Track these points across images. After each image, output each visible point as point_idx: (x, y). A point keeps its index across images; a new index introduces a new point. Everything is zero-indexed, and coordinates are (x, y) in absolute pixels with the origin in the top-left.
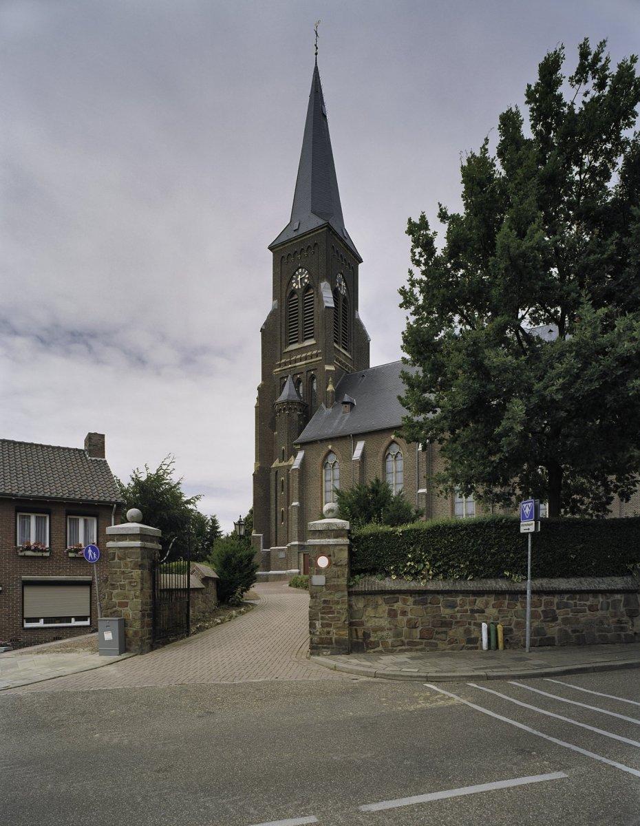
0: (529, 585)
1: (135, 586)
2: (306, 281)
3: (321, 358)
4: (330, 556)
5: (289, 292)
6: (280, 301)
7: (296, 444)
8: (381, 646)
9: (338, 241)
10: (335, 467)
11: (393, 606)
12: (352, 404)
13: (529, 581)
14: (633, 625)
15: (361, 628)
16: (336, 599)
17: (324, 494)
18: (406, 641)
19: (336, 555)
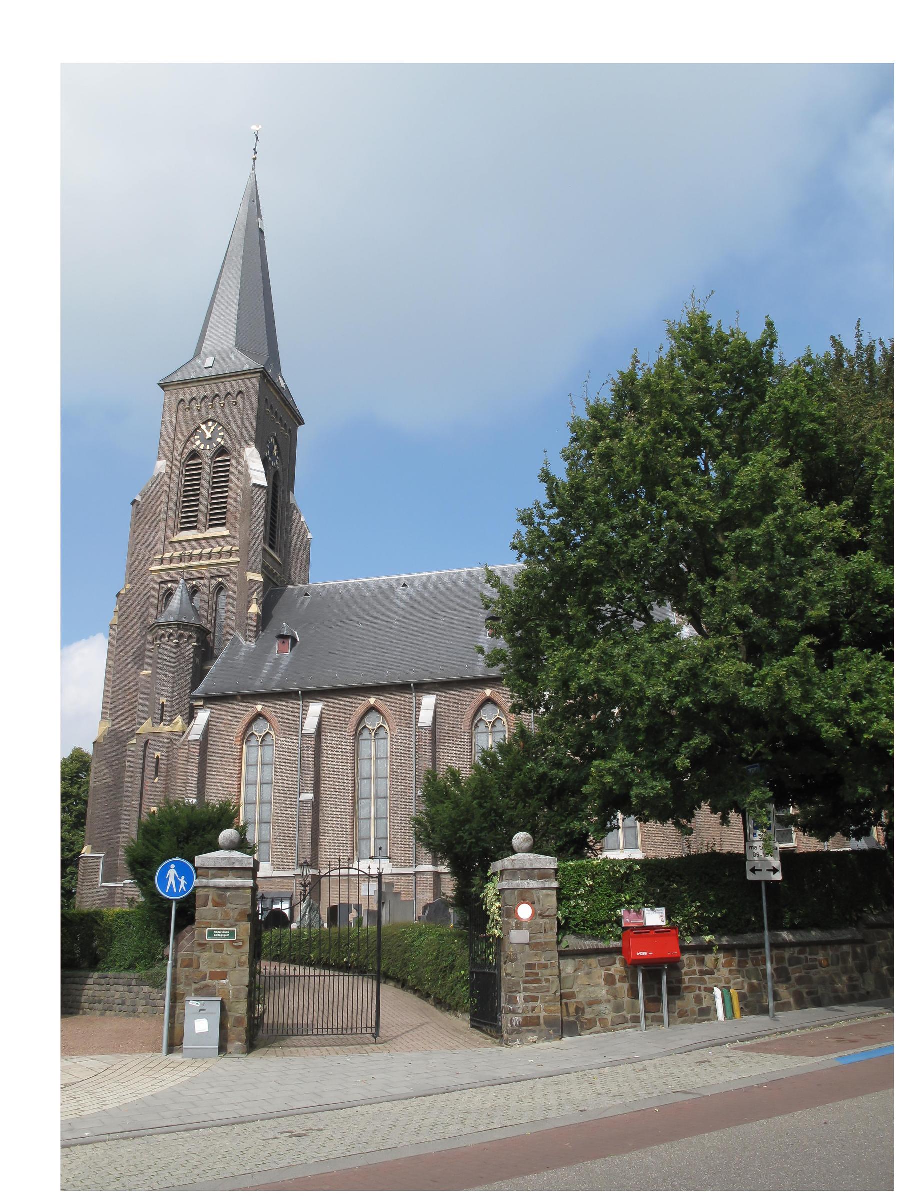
1: (239, 947)
3: (238, 559)
4: (533, 903)
5: (188, 450)
7: (197, 699)
8: (598, 1024)
9: (275, 394)
10: (264, 743)
11: (610, 970)
12: (294, 641)
13: (767, 933)
14: (864, 982)
15: (573, 1001)
16: (543, 962)
18: (629, 1016)
19: (541, 902)
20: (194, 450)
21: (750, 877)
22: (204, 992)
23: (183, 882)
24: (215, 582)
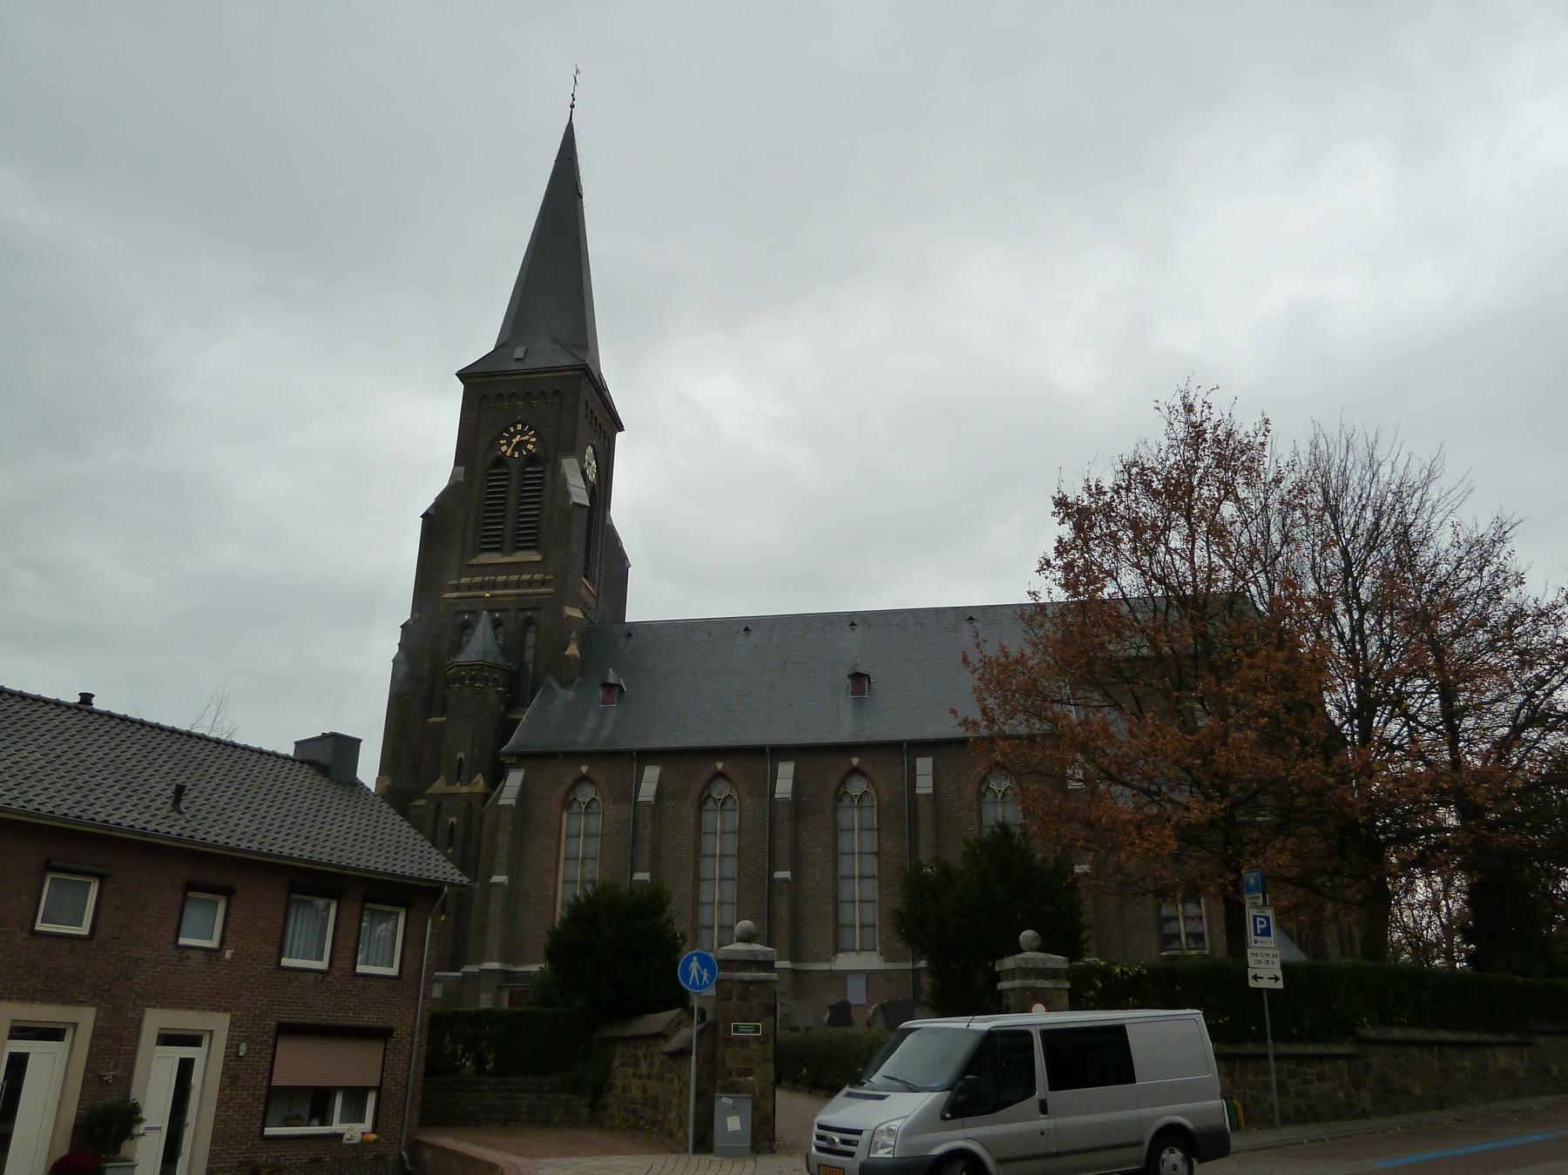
0: (1271, 1048)
1: (764, 1043)
2: (530, 447)
6: (469, 472)
9: (595, 394)
10: (589, 810)
17: (562, 864)
20: (499, 456)
21: (1252, 984)
22: (731, 1089)
23: (705, 974)
24: (522, 616)
